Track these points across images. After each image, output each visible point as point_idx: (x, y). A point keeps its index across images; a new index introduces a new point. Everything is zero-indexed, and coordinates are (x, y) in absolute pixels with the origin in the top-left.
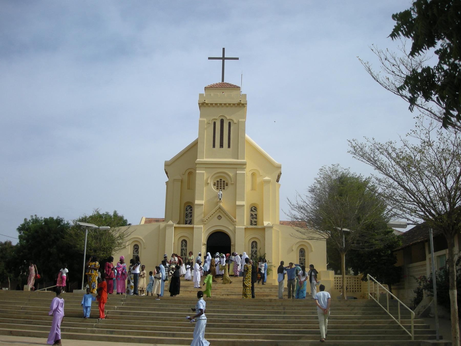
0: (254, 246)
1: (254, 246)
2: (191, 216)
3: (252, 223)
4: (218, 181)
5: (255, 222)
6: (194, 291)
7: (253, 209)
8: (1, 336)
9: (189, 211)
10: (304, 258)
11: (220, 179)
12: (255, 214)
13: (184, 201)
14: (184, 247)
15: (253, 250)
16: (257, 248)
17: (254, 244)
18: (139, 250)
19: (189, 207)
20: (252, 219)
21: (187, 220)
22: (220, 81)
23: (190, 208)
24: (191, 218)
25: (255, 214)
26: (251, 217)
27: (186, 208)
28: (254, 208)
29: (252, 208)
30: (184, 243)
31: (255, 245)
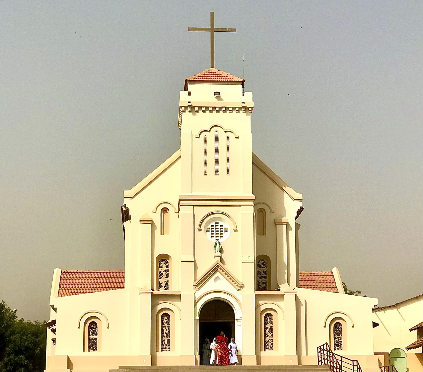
2: (167, 276)
5: (264, 283)
6: (406, 364)
9: (164, 268)
10: (340, 337)
11: (216, 223)
12: (264, 272)
13: (156, 255)
18: (98, 330)
20: (259, 279)
25: (264, 272)
26: (259, 275)
28: (261, 262)
31: (269, 319)
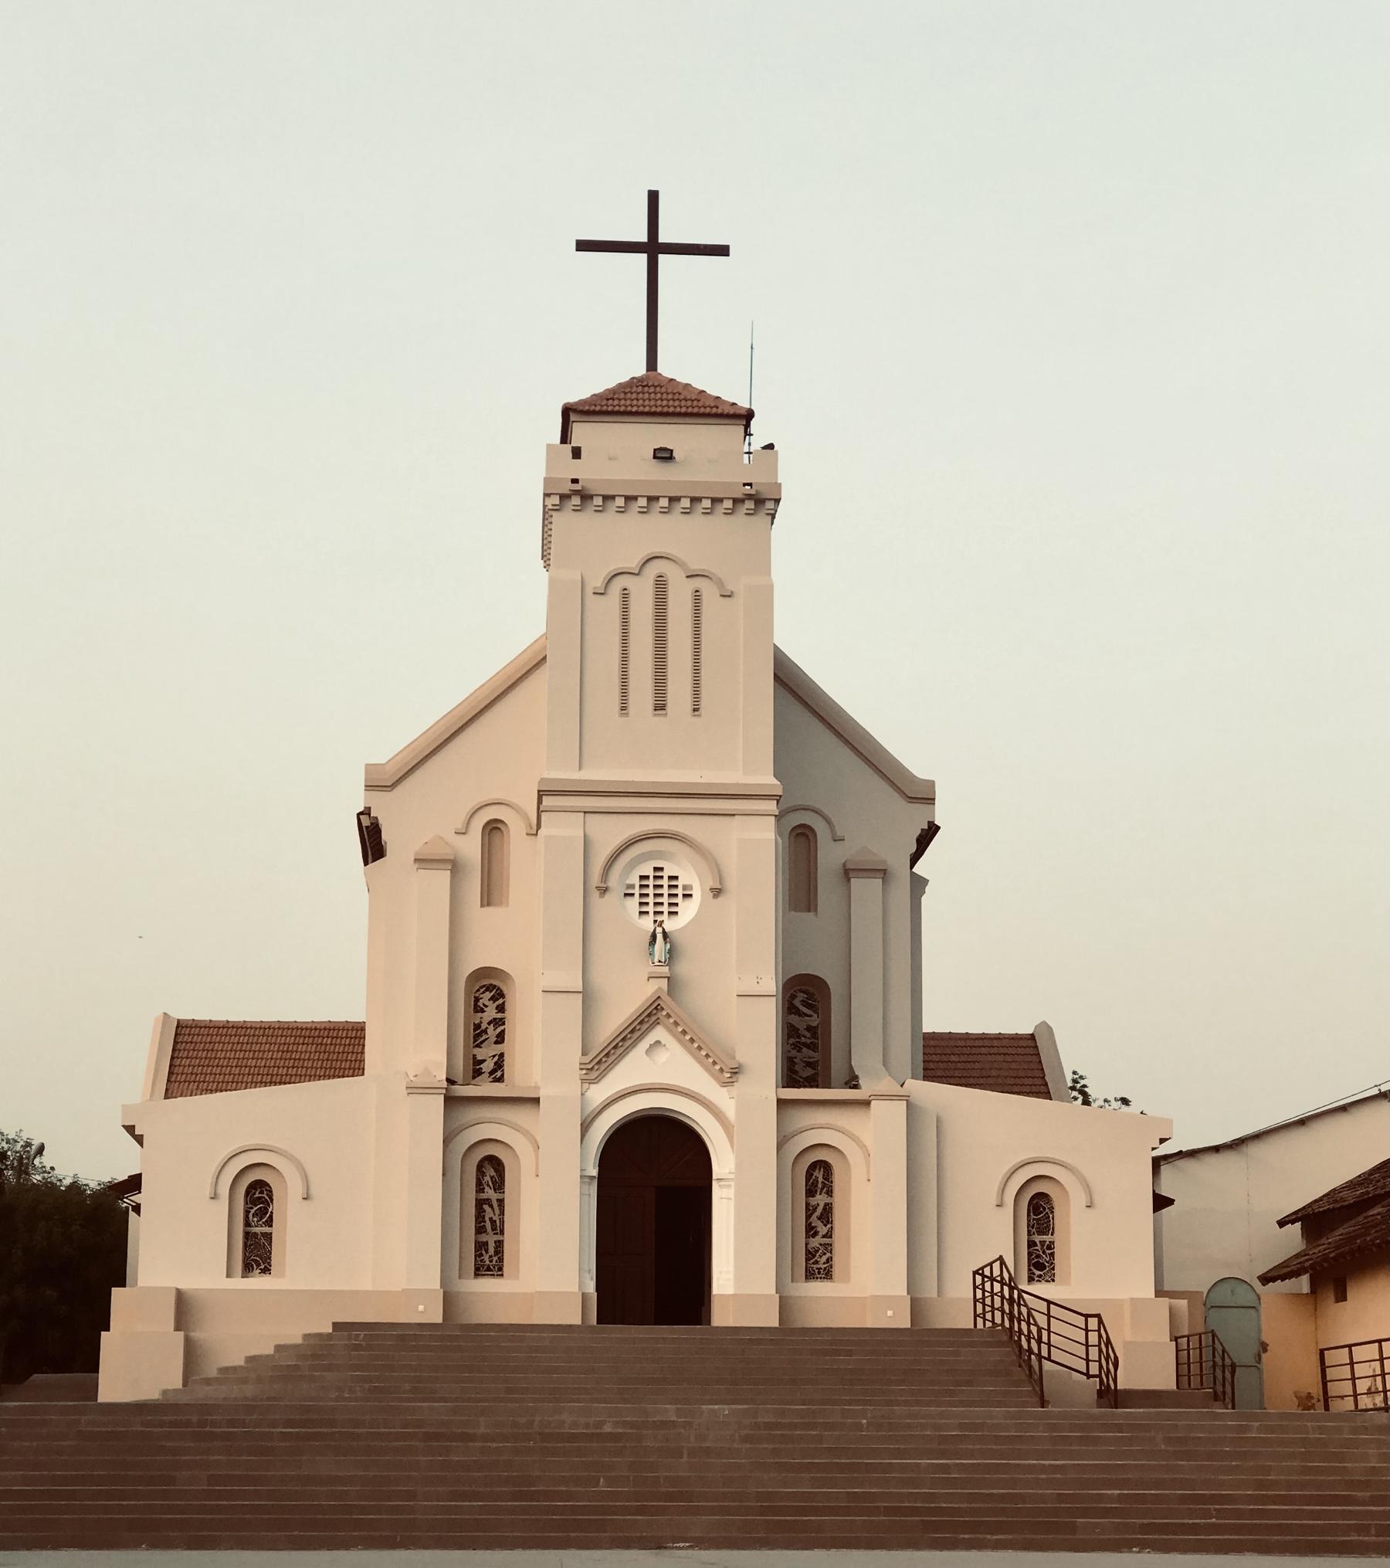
0: (820, 1185)
1: (820, 1185)
2: (500, 1039)
3: (796, 1072)
4: (647, 877)
5: (809, 1064)
7: (797, 1002)
8: (2, 1552)
9: (491, 1013)
10: (1047, 1238)
11: (656, 869)
12: (809, 1028)
14: (490, 1193)
15: (813, 1201)
16: (830, 1193)
17: (819, 1175)
18: (276, 1208)
19: (488, 995)
20: (794, 1053)
21: (479, 1058)
22: (640, 369)
23: (493, 999)
24: (498, 1049)
26: (791, 1041)
27: (477, 999)
28: (801, 996)
29: (793, 997)
30: (490, 1172)
31: (821, 1180)
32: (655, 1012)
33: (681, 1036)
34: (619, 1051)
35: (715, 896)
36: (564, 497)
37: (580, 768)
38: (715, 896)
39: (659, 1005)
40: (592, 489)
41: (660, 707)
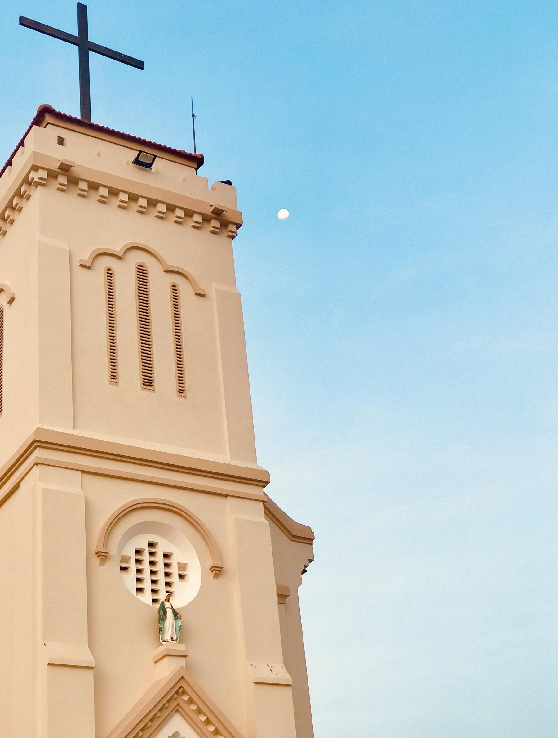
11: (151, 545)
32: (176, 696)
33: (203, 727)
34: (157, 722)
35: (216, 576)
36: (52, 175)
37: (74, 428)
38: (216, 576)
39: (181, 687)
40: (77, 171)
41: (148, 382)
